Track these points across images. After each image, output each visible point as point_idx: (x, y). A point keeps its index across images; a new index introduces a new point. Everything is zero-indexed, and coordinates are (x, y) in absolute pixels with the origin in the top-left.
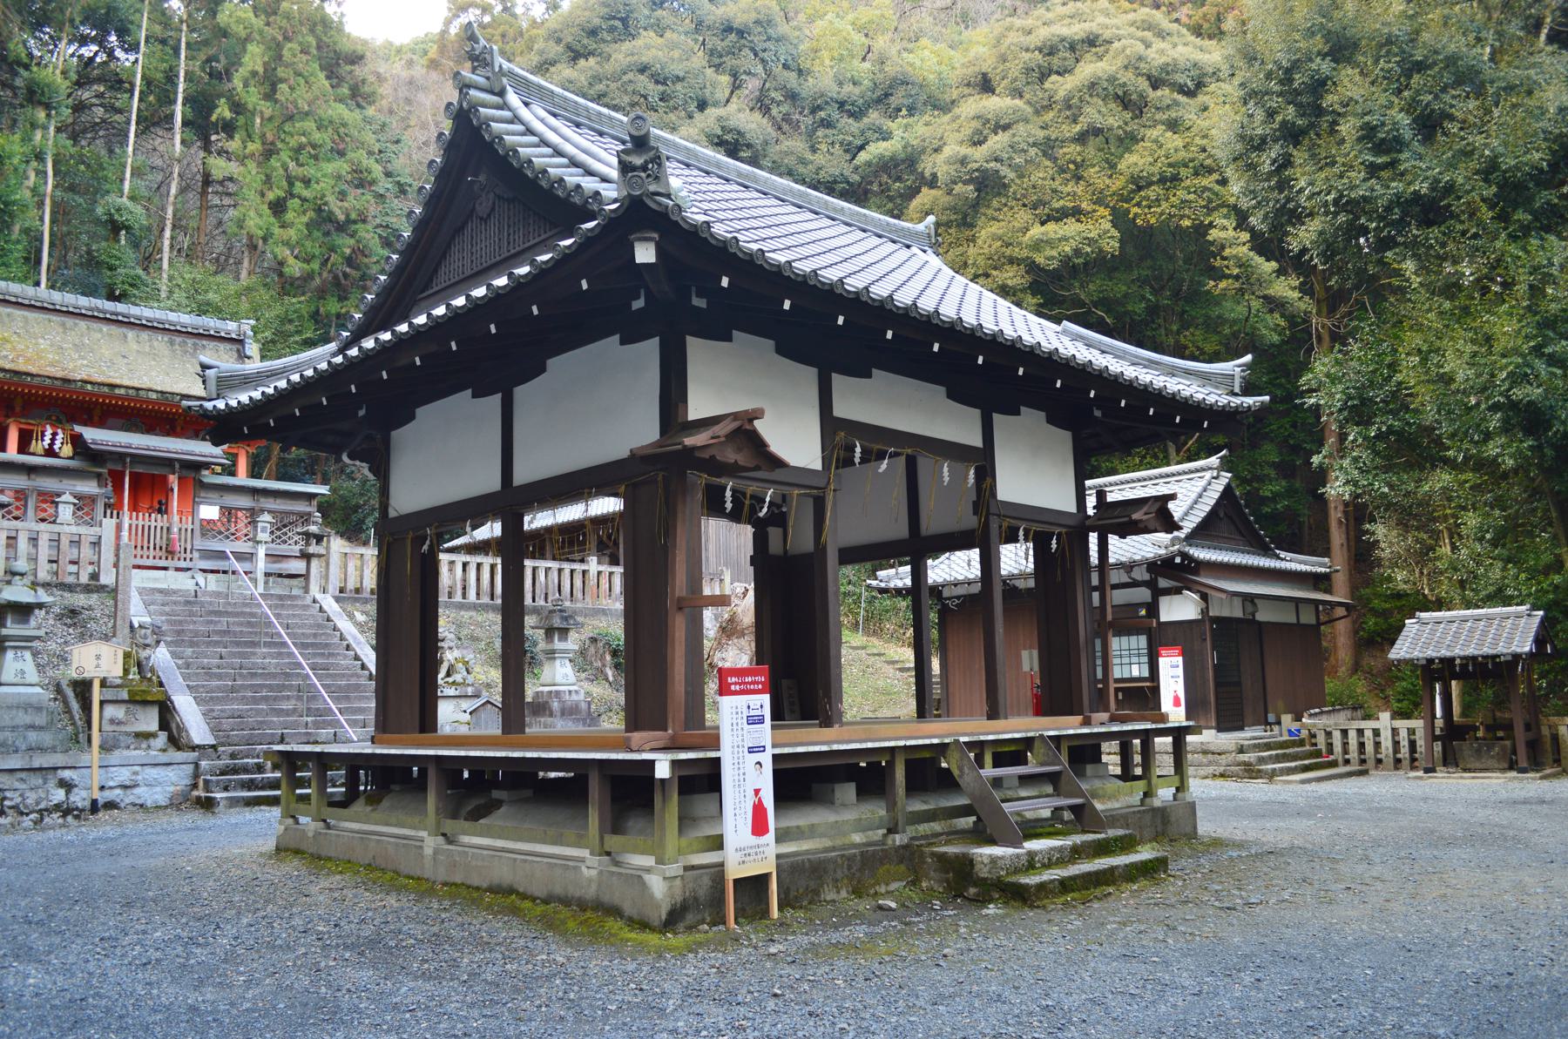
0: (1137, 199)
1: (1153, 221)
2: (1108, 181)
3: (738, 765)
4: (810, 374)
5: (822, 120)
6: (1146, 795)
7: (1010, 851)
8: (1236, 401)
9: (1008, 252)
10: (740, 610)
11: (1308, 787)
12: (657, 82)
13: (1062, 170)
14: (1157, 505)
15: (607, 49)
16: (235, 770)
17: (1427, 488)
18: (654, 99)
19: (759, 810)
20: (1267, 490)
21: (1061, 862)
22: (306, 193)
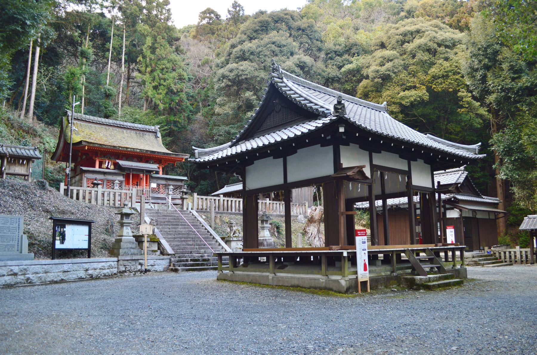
0: (435, 83)
1: (440, 90)
2: (425, 77)
3: (360, 253)
4: (367, 153)
5: (330, 57)
6: (453, 266)
7: (424, 277)
8: (477, 156)
9: (393, 100)
10: (314, 215)
11: (496, 268)
12: (278, 47)
13: (409, 74)
14: (455, 186)
15: (261, 37)
16: (181, 261)
17: (530, 176)
18: (278, 52)
19: (365, 265)
20: (476, 175)
21: (437, 280)
22: (165, 84)
